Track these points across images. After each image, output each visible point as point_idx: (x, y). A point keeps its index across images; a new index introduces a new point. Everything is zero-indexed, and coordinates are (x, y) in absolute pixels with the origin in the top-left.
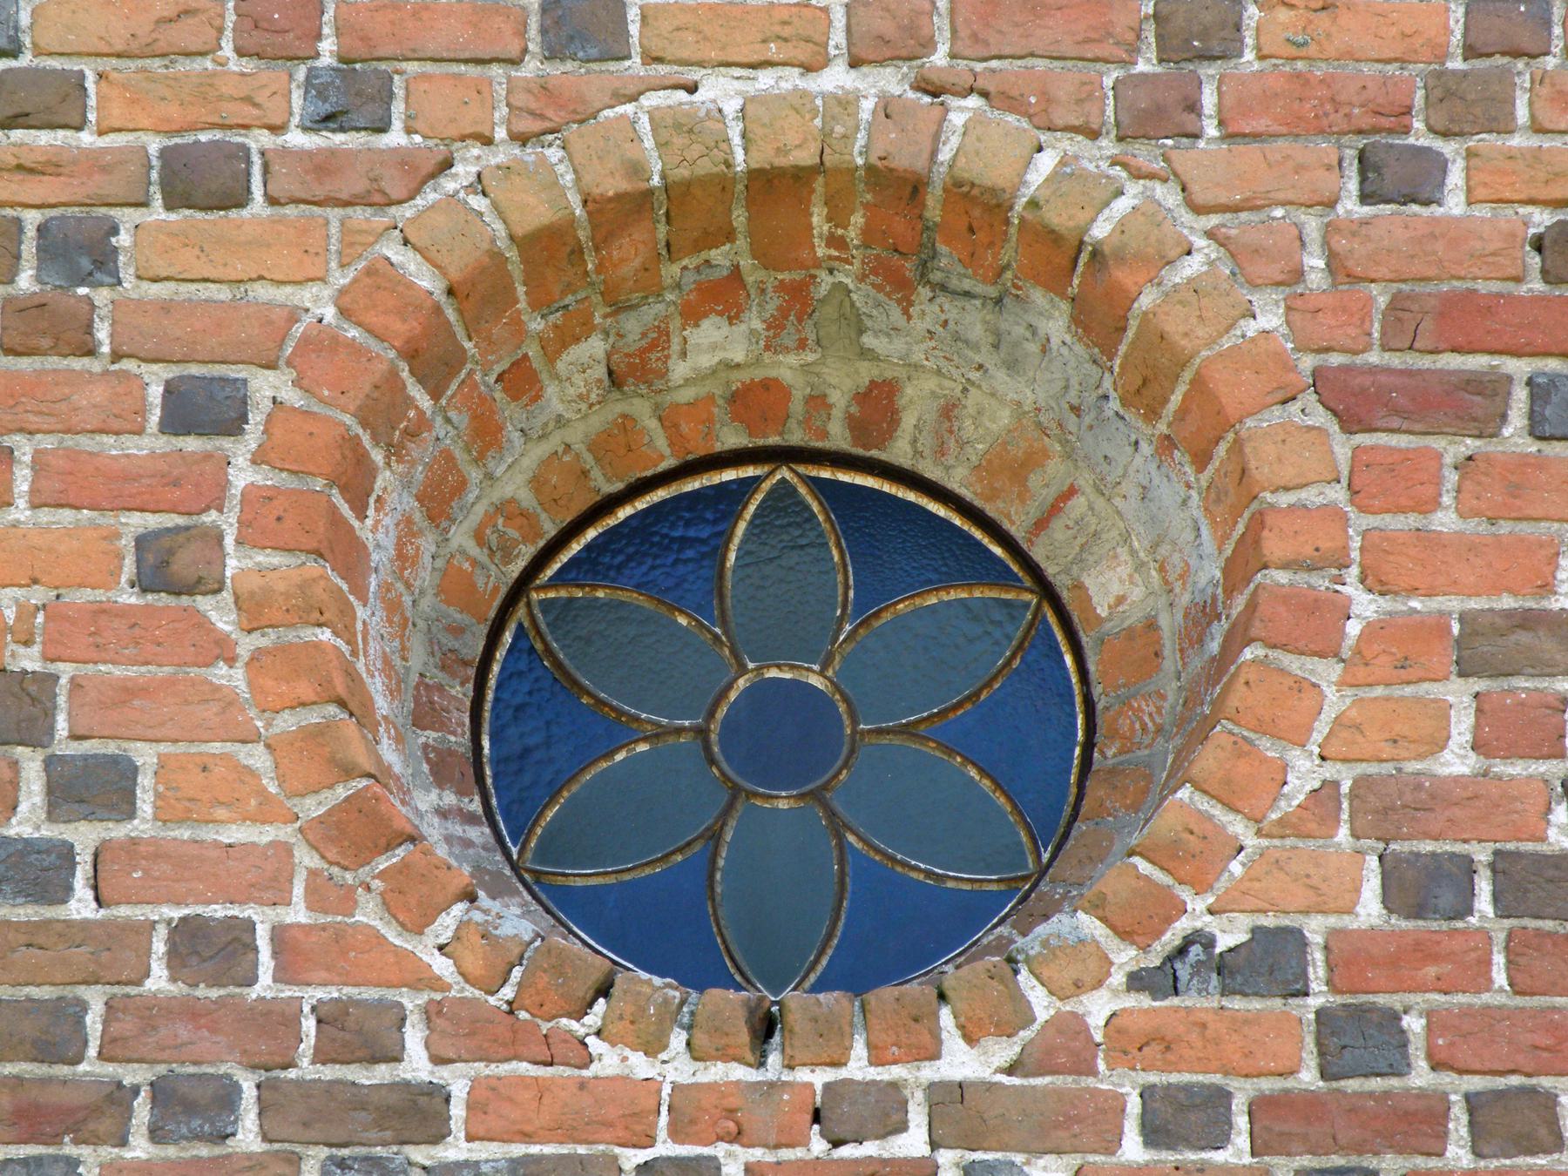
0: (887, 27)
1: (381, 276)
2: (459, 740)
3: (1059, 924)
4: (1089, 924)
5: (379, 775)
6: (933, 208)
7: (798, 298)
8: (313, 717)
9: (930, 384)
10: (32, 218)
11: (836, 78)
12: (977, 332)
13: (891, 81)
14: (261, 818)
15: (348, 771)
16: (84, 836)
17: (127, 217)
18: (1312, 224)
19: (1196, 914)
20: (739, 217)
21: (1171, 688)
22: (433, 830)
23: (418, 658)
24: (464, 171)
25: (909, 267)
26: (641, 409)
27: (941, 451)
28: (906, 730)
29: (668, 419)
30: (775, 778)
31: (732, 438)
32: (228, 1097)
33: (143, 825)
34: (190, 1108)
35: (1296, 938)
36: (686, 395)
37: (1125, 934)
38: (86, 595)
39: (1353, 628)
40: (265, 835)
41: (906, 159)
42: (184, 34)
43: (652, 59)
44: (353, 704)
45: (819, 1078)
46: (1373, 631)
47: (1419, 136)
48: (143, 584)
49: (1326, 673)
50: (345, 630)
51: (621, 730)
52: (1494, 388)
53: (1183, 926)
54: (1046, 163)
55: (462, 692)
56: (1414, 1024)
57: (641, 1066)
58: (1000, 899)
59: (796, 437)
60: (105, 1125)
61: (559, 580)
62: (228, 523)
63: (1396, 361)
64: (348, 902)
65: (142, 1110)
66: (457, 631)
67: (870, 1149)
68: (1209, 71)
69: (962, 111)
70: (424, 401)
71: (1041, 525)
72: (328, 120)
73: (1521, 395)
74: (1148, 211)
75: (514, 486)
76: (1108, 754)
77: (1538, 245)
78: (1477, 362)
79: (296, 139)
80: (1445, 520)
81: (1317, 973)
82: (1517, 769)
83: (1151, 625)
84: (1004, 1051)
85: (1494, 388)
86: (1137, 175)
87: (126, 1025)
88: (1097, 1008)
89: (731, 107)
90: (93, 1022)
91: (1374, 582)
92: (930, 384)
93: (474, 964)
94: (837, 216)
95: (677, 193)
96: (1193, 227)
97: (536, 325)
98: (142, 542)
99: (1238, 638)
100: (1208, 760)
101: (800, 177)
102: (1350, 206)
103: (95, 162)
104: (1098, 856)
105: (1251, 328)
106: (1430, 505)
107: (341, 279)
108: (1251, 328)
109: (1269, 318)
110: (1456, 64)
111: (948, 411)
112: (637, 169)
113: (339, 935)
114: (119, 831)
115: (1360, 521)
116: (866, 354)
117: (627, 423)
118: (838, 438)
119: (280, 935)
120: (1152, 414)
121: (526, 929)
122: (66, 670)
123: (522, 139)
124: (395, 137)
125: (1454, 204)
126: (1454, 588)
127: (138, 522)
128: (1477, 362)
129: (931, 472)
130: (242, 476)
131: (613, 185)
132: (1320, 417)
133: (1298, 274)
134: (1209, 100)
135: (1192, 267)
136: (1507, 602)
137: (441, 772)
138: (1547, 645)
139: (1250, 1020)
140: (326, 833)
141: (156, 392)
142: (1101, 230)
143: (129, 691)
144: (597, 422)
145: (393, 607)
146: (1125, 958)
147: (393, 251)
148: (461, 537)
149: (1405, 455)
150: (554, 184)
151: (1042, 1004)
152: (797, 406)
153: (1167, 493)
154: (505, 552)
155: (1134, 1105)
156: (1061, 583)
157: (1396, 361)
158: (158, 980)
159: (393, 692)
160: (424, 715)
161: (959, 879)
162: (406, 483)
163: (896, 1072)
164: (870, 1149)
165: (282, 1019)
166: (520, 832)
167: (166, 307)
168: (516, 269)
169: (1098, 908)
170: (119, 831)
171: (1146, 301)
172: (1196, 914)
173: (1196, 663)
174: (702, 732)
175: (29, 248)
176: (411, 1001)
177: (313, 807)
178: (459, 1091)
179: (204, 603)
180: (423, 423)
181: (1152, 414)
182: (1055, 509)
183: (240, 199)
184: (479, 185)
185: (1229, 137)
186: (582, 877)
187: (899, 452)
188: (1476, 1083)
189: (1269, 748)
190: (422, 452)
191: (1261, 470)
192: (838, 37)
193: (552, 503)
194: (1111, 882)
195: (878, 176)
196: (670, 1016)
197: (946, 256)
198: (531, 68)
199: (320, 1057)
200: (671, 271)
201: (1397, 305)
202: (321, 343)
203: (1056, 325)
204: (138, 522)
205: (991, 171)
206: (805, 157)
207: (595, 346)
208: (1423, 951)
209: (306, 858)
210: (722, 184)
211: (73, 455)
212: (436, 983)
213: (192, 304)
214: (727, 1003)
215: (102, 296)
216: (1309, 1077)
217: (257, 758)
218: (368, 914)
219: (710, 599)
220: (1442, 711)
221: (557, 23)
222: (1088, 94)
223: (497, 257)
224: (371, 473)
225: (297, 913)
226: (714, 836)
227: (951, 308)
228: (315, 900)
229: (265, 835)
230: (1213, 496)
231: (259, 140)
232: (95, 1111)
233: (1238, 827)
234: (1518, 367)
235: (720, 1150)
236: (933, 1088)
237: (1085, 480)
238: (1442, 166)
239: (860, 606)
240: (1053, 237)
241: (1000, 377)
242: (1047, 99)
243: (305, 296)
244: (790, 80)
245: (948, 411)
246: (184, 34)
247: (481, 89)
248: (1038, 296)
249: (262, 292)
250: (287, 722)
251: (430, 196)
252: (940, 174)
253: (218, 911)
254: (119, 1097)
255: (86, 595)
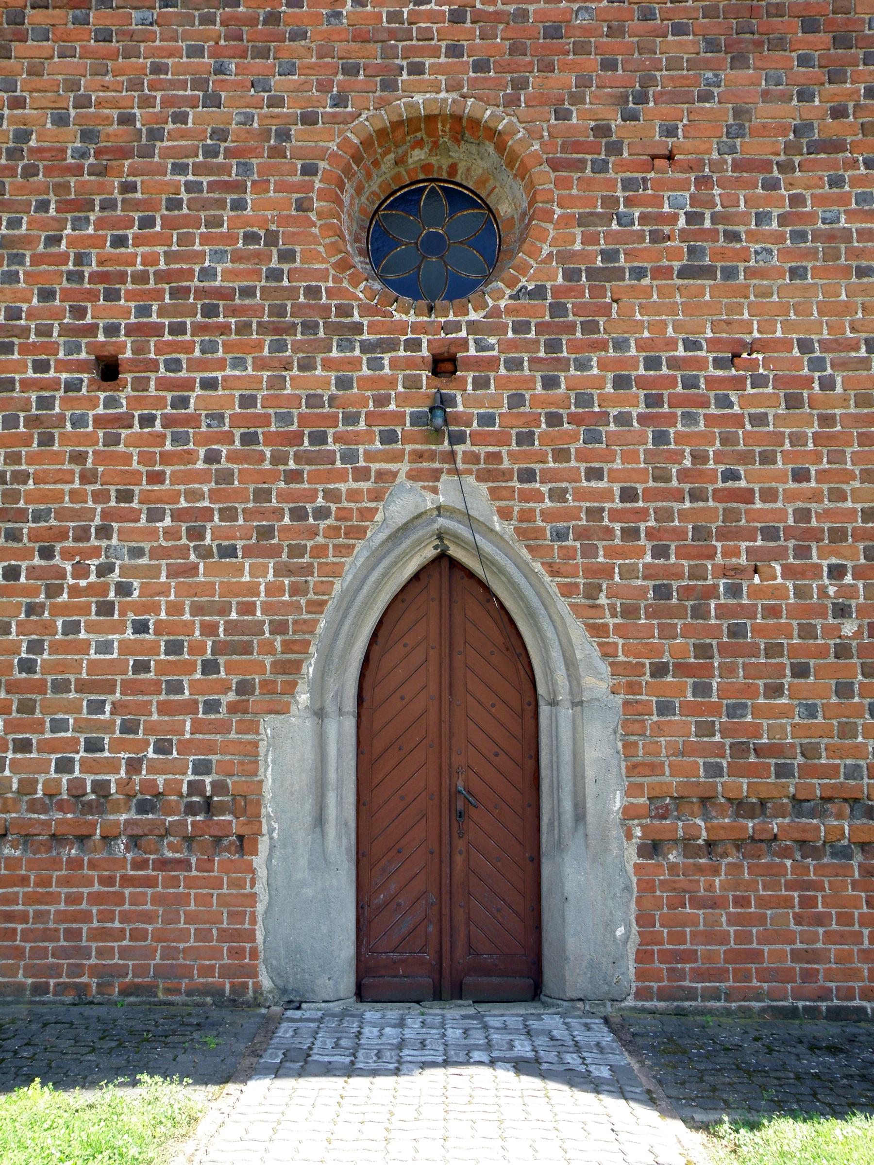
0: (454, 83)
1: (346, 140)
2: (364, 246)
3: (494, 284)
4: (500, 284)
5: (347, 252)
6: (464, 124)
7: (435, 144)
8: (333, 239)
9: (464, 163)
10: (274, 128)
11: (443, 95)
12: (474, 151)
13: (455, 95)
14: (322, 262)
15: (340, 252)
16: (286, 267)
17: (293, 127)
18: (545, 125)
19: (523, 282)
20: (423, 126)
21: (517, 232)
22: (359, 266)
23: (355, 227)
24: (364, 116)
25: (459, 137)
26: (402, 170)
27: (467, 179)
28: (460, 242)
29: (408, 172)
30: (433, 254)
31: (422, 176)
32: (317, 325)
33: (298, 264)
34: (309, 328)
35: (544, 287)
36: (412, 167)
37: (508, 287)
38: (285, 212)
39: (556, 216)
40: (324, 266)
41: (458, 112)
42: (306, 87)
43: (403, 91)
44: (341, 236)
45: (443, 320)
46: (560, 217)
47: (567, 105)
48: (297, 210)
49: (550, 227)
50: (339, 220)
51: (399, 243)
52: (584, 162)
53: (520, 284)
54: (488, 112)
55: (364, 235)
56: (569, 306)
57: (404, 317)
58: (481, 281)
59: (435, 176)
60: (292, 332)
61: (385, 209)
62: (314, 196)
63: (563, 156)
64: (341, 282)
65: (299, 327)
66: (363, 221)
67: (454, 335)
68: (522, 92)
69: (470, 101)
70: (356, 168)
71: (489, 195)
72: (335, 106)
73: (589, 163)
74: (510, 123)
75: (375, 188)
76: (504, 247)
77: (592, 129)
78: (580, 156)
79: (328, 110)
80: (574, 192)
81: (549, 295)
82: (590, 248)
83: (513, 217)
84: (483, 313)
85: (584, 162)
86: (508, 115)
87: (296, 309)
88: (503, 303)
89: (421, 101)
90: (289, 308)
91: (560, 206)
92: (464, 163)
93: (368, 295)
94: (444, 126)
95: (410, 120)
96: (520, 126)
97: (379, 151)
98: (296, 200)
99: (531, 219)
100: (525, 247)
101: (436, 117)
102: (553, 121)
103: (287, 115)
104: (502, 270)
105: (533, 149)
106: (571, 188)
107: (338, 141)
108: (533, 149)
109: (536, 147)
110: (574, 90)
111: (468, 169)
112: (401, 115)
113: (339, 289)
114: (293, 266)
115: (556, 192)
116: (450, 157)
117: (399, 173)
118: (445, 176)
119: (327, 288)
120: (512, 169)
121: (379, 287)
122: (281, 229)
123: (376, 109)
124: (349, 109)
125: (574, 121)
126: (576, 207)
127: (296, 196)
128: (580, 156)
129: (465, 184)
130: (317, 185)
131: (396, 119)
132: (548, 169)
133: (542, 137)
134: (522, 98)
135: (520, 135)
136: (588, 210)
137: (360, 253)
138: (596, 220)
139: (536, 305)
140: (336, 266)
141: (299, 166)
142: (500, 127)
143: (294, 234)
144: (393, 172)
145: (349, 215)
146: (508, 292)
147: (349, 134)
148: (363, 199)
149: (566, 177)
150: (383, 118)
151: (490, 302)
152: (436, 169)
153: (516, 187)
154: (373, 203)
155: (510, 325)
156: (493, 208)
157: (563, 156)
158: (302, 299)
159: (350, 235)
160: (357, 240)
161: (473, 276)
162: (352, 186)
163: (460, 318)
164: (454, 335)
165: (327, 308)
166: (377, 266)
167: (301, 147)
168: (375, 138)
169: (502, 281)
170: (293, 266)
171: (510, 143)
172: (523, 282)
173: (523, 225)
174: (416, 243)
175: (273, 135)
176: (355, 304)
177: (333, 260)
178: (366, 323)
179: (310, 214)
180: (355, 173)
181: (512, 169)
182: (492, 191)
183: (317, 123)
184: (367, 119)
185: (527, 106)
186: (391, 277)
187: (458, 179)
188: (582, 319)
189: (538, 244)
190: (355, 180)
191: (536, 181)
192: (443, 86)
193: (383, 191)
194: (505, 275)
195: (452, 116)
196: (410, 306)
197: (467, 134)
198: (378, 93)
199: (336, 316)
200: (408, 138)
201: (563, 143)
202: (334, 155)
203: (491, 149)
204: (296, 196)
205: (476, 115)
206: (437, 112)
207: (392, 156)
208: (571, 289)
209: (332, 272)
210: (419, 118)
211: (282, 181)
212: (360, 299)
213: (307, 147)
214: (423, 303)
215: (288, 145)
216: (547, 318)
217: (321, 249)
218: (345, 284)
219: (417, 212)
220: (575, 235)
221: (710, 845)
222: (497, 97)
223: (371, 135)
224: (344, 184)
225: (331, 284)
226: (419, 267)
227: (469, 146)
228: (334, 281)
229: (324, 266)
230: (525, 187)
231: (320, 110)
232: (289, 328)
233: (532, 262)
234: (589, 157)
235: (422, 336)
236: (467, 322)
237: (498, 185)
238: (571, 112)
239: (450, 213)
240: (490, 129)
241: (479, 161)
242: (488, 99)
243: (330, 144)
244: (434, 95)
245: (468, 169)
246: (306, 87)
247: (368, 98)
248: (487, 143)
249: (321, 144)
250: (327, 241)
251: (357, 122)
252: (466, 115)
253: (314, 284)
254: (295, 325)
255: (285, 212)
